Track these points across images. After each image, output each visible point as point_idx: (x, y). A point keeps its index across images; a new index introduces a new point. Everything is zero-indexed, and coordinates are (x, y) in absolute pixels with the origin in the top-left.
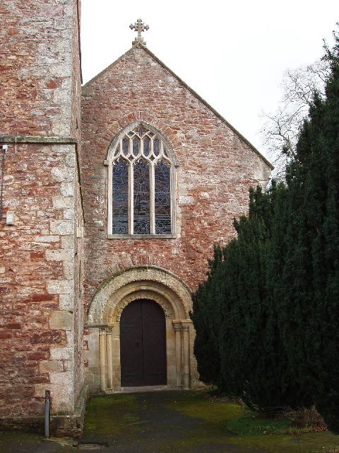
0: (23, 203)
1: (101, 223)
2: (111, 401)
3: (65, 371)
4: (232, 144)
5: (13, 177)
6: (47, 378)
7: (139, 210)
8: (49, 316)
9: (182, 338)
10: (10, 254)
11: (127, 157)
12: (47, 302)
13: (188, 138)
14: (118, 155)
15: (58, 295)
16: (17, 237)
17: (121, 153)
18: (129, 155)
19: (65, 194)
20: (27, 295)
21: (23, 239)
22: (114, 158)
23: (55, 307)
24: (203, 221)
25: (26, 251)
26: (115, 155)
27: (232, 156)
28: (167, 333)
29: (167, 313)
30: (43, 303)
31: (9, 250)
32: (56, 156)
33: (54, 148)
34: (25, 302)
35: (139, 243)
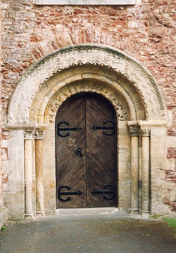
9: (140, 145)
28: (55, 175)
29: (119, 112)
35: (81, 12)
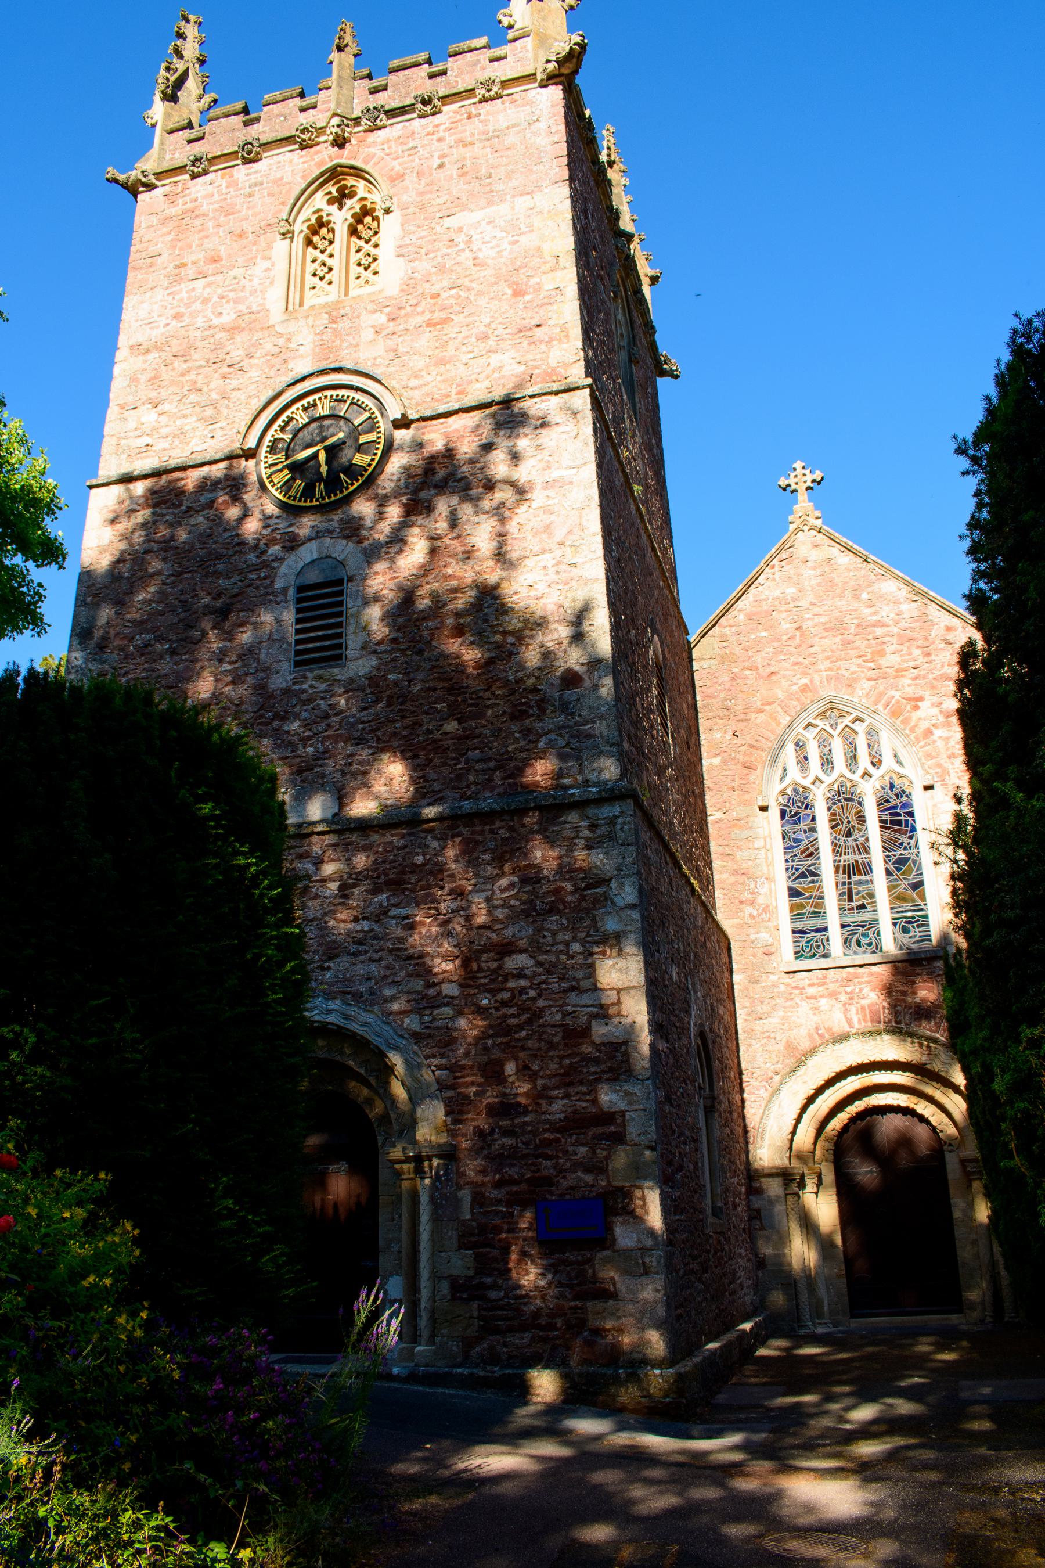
0: (539, 930)
1: (764, 936)
2: (940, 1365)
6: (612, 1288)
7: (850, 899)
8: (608, 1158)
10: (524, 1033)
11: (807, 783)
12: (601, 1130)
14: (788, 781)
15: (623, 1113)
16: (534, 999)
17: (794, 774)
18: (811, 778)
19: (620, 902)
20: (562, 1116)
21: (547, 1003)
22: (780, 787)
23: (619, 1138)
25: (553, 1026)
30: (593, 1131)
31: (520, 1027)
32: (596, 826)
33: (591, 811)
34: (558, 1131)
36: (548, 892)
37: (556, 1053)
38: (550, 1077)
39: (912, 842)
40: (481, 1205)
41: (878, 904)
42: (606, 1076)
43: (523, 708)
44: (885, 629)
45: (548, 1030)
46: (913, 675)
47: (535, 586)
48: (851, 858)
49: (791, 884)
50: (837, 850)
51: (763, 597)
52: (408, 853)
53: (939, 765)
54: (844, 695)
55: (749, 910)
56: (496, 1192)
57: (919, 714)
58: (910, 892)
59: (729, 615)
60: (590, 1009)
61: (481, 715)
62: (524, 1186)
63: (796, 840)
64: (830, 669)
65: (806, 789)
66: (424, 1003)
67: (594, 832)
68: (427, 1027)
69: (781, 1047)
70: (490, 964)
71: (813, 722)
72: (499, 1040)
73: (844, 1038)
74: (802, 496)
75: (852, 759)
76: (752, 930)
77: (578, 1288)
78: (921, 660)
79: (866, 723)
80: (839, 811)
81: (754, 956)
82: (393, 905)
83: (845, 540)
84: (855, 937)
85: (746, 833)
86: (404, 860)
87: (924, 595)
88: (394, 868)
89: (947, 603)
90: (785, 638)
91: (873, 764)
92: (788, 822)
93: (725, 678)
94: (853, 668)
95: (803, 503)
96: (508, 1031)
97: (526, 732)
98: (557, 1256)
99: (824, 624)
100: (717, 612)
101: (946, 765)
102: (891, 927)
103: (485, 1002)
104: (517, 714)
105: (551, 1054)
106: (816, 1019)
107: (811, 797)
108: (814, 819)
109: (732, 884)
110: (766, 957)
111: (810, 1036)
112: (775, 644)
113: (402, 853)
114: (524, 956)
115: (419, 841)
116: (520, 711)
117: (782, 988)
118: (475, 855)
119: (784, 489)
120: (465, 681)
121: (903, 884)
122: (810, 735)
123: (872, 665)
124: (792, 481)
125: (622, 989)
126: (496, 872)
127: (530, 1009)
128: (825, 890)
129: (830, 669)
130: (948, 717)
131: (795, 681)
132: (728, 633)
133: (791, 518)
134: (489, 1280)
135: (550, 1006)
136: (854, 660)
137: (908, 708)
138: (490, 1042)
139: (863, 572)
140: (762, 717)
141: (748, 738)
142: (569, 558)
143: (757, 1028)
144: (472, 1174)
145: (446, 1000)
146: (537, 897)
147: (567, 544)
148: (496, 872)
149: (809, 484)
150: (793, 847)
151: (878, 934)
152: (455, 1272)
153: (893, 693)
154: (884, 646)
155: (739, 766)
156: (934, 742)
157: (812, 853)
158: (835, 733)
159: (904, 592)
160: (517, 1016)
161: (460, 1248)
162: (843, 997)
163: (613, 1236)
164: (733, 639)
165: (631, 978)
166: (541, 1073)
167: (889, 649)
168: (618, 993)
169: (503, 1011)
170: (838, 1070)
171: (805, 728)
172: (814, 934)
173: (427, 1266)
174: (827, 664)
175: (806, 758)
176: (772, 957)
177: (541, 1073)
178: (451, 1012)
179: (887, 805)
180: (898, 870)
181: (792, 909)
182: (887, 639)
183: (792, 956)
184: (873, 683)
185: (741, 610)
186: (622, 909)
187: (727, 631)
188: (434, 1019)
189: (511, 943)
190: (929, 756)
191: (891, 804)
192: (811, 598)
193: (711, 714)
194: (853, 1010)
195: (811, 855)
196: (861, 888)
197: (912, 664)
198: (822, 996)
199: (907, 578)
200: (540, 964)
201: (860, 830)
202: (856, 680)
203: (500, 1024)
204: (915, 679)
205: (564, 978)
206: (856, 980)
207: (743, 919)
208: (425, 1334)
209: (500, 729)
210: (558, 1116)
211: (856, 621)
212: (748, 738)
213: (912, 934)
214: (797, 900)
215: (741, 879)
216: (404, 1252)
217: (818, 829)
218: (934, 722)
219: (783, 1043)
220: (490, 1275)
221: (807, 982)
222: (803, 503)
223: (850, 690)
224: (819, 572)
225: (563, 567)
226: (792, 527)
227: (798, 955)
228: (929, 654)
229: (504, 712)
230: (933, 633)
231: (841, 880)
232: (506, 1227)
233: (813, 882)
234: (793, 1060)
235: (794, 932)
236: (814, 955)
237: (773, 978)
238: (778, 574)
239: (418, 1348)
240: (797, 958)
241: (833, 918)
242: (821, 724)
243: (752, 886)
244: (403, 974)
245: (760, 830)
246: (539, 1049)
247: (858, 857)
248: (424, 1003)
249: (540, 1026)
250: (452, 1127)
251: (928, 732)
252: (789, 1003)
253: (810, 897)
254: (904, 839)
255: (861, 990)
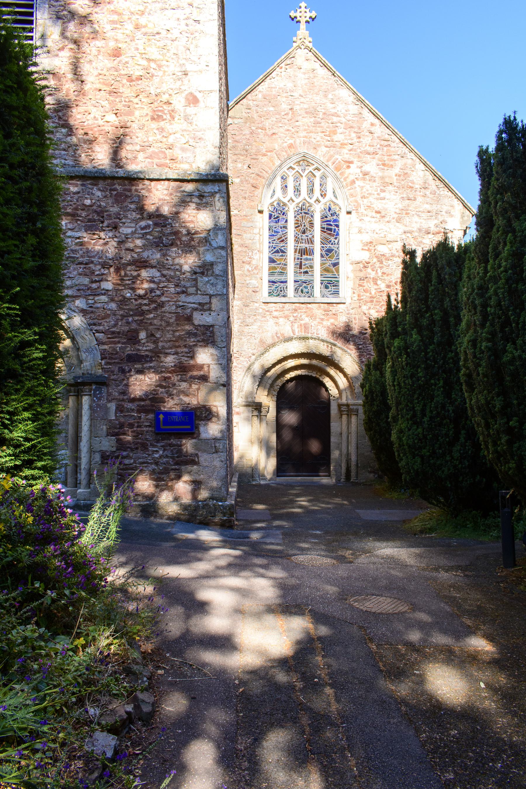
1: (254, 282)
3: (216, 452)
4: (421, 182)
5: (151, 223)
6: (197, 460)
7: (301, 267)
10: (152, 316)
11: (285, 200)
13: (365, 174)
14: (275, 198)
16: (159, 296)
17: (279, 194)
18: (288, 198)
19: (214, 244)
20: (173, 364)
24: (379, 282)
25: (170, 313)
26: (272, 197)
27: (420, 199)
31: (150, 312)
32: (203, 196)
34: (170, 372)
36: (171, 233)
37: (171, 328)
38: (166, 342)
39: (336, 241)
40: (122, 411)
41: (315, 272)
42: (201, 344)
43: (160, 114)
44: (338, 118)
45: (167, 315)
46: (350, 148)
47: (171, 31)
48: (304, 246)
49: (271, 256)
50: (297, 240)
51: (273, 86)
52: (80, 197)
53: (356, 201)
54: (311, 152)
55: (247, 267)
56: (131, 405)
57: (348, 171)
58: (332, 267)
59: (253, 93)
60: (192, 305)
61: (131, 113)
62: (148, 402)
63: (275, 232)
64: (306, 137)
65: (285, 204)
66: (89, 292)
67: (202, 200)
68: (91, 307)
69: (257, 341)
70: (132, 272)
71: (293, 166)
72: (136, 318)
73: (290, 339)
74: (303, 26)
75: (311, 191)
76: (248, 278)
77: (177, 459)
78: (355, 140)
79: (321, 172)
80: (300, 219)
81: (247, 292)
82: (70, 229)
83: (324, 59)
84: (301, 288)
85: (250, 224)
86: (77, 201)
87: (362, 102)
88: (71, 205)
89: (374, 109)
90: (283, 113)
91: (322, 196)
92: (272, 221)
93: (247, 132)
94: (318, 138)
95: (303, 31)
96: (142, 313)
97: (162, 130)
98: (166, 441)
99: (306, 109)
100: (247, 90)
101: (359, 201)
102: (320, 285)
103: (128, 295)
104: (156, 117)
105: (168, 329)
106: (276, 328)
107: (287, 209)
108: (286, 221)
109: (239, 252)
110: (254, 294)
111: (273, 337)
112: (277, 116)
113: (76, 196)
114: (154, 270)
115: (88, 190)
116: (158, 115)
117: (261, 311)
118: (125, 204)
119: (293, 19)
120: (121, 88)
121: (328, 263)
122: (291, 173)
123: (329, 138)
124: (298, 14)
125: (213, 295)
126: (139, 216)
127: (156, 301)
128: (288, 261)
129: (306, 137)
130: (364, 175)
131: (286, 140)
132: (251, 104)
133: (294, 39)
134: (125, 453)
135: (169, 301)
136: (319, 134)
137: (345, 166)
138: (130, 319)
139: (331, 81)
140: (265, 159)
141: (256, 169)
142: (195, 17)
143: (245, 330)
144: (117, 394)
145: (103, 292)
146: (164, 235)
147: (194, 6)
148: (139, 216)
149: (308, 19)
150: (273, 235)
151: (313, 288)
152: (104, 449)
153: (337, 156)
154: (337, 128)
155: (250, 185)
156: (355, 188)
157: (283, 240)
158: (304, 175)
159: (352, 98)
160: (148, 305)
161: (108, 435)
162: (292, 319)
163: (199, 431)
164: (254, 108)
165: (218, 289)
166: (161, 339)
167: (339, 131)
168: (210, 298)
169: (140, 301)
170: (285, 355)
171: (288, 169)
172: (279, 284)
173: (86, 445)
174: (304, 134)
175: (286, 186)
176: (257, 294)
177: (161, 339)
178: (107, 299)
179: (325, 219)
180: (327, 255)
181: (269, 270)
182: (338, 124)
183: (267, 294)
184: (328, 149)
185: (260, 92)
186: (215, 248)
187: (251, 103)
188: (95, 302)
189: (146, 261)
190: (352, 195)
191: (328, 219)
192: (300, 92)
193: (237, 152)
194: (296, 325)
195: (283, 241)
196: (307, 262)
197: (350, 142)
198: (281, 317)
199: (355, 90)
200: (164, 276)
201: (310, 231)
202: (319, 146)
203: (137, 309)
204: (351, 150)
205: (178, 286)
206: (299, 311)
207: (243, 271)
208: (84, 482)
209: (144, 125)
210: (170, 364)
211: (323, 111)
212: (256, 169)
213: (330, 289)
214: (273, 265)
215: (244, 249)
216: (69, 437)
217: (289, 227)
218: (357, 176)
219: (258, 340)
220: (125, 451)
221: (274, 309)
222: (303, 31)
223: (315, 151)
224: (307, 76)
225: (190, 22)
226: (295, 45)
227: (270, 294)
228: (359, 138)
229: (147, 114)
230: (364, 126)
231: (297, 257)
232: (136, 425)
233: (282, 256)
234: (263, 348)
235: (269, 282)
236: (279, 295)
237: (256, 304)
238: (283, 73)
239: (79, 491)
240: (269, 296)
241: (291, 276)
242: (297, 168)
243: (250, 254)
244: (75, 273)
245: (257, 224)
246: (161, 325)
247: (307, 246)
248: (89, 292)
249: (162, 312)
250: (105, 367)
251: (353, 182)
252: (263, 319)
253: (280, 264)
254: (332, 239)
255: (301, 316)
